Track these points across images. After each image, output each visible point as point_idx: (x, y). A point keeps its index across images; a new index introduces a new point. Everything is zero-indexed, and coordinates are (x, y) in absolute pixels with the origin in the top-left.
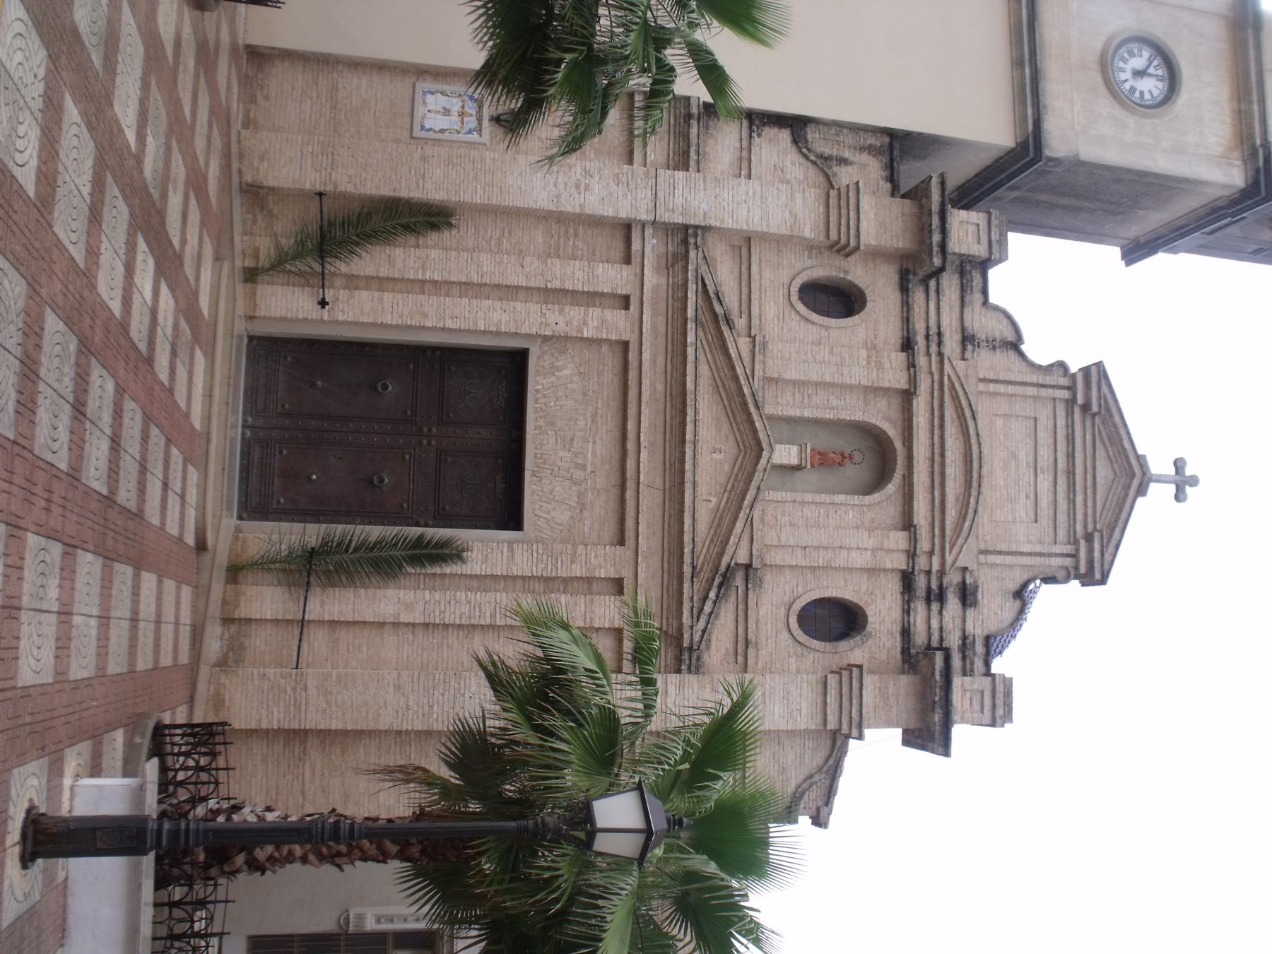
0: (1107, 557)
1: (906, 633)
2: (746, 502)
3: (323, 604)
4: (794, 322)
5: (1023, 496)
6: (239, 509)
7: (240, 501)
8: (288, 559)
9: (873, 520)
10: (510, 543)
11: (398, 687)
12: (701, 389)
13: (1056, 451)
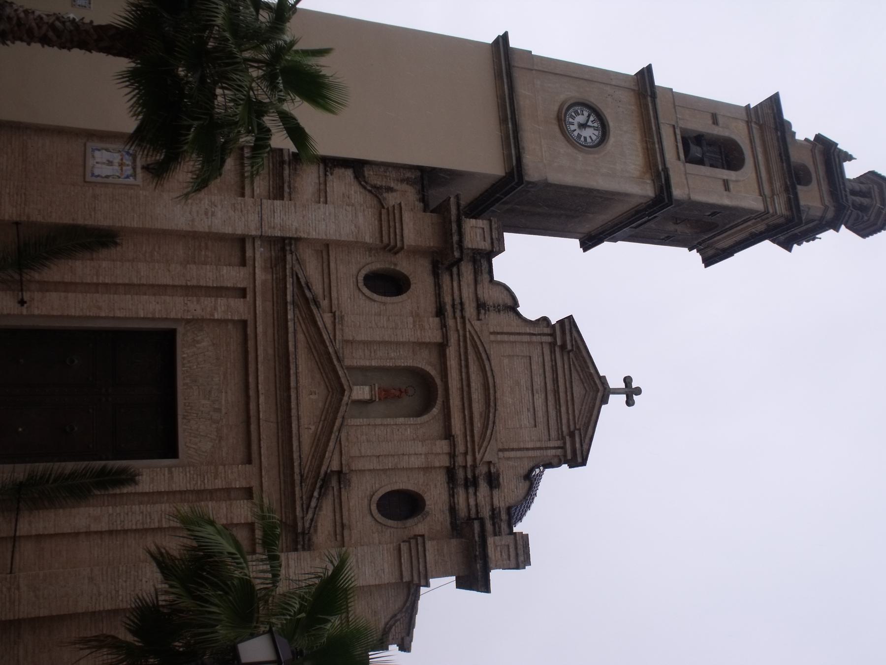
0: (585, 447)
1: (453, 510)
2: (335, 428)
5: (525, 410)
13: (545, 377)
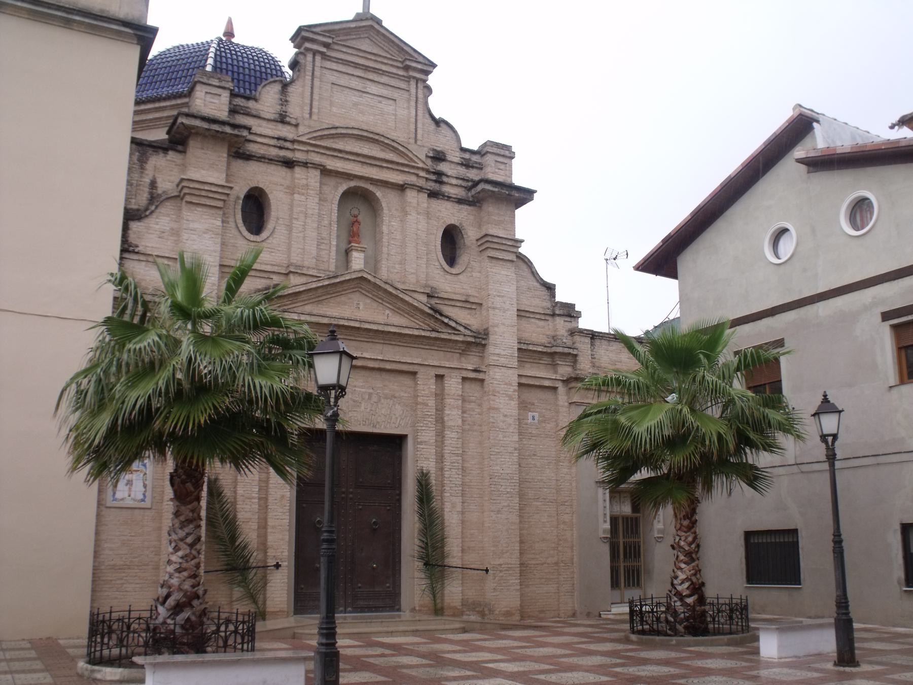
0: (421, 59)
1: (460, 201)
2: (394, 292)
3: (453, 557)
4: (274, 241)
5: (379, 105)
6: (393, 611)
7: (389, 611)
8: (431, 577)
9: (396, 210)
10: (416, 442)
11: (499, 512)
12: (328, 313)
